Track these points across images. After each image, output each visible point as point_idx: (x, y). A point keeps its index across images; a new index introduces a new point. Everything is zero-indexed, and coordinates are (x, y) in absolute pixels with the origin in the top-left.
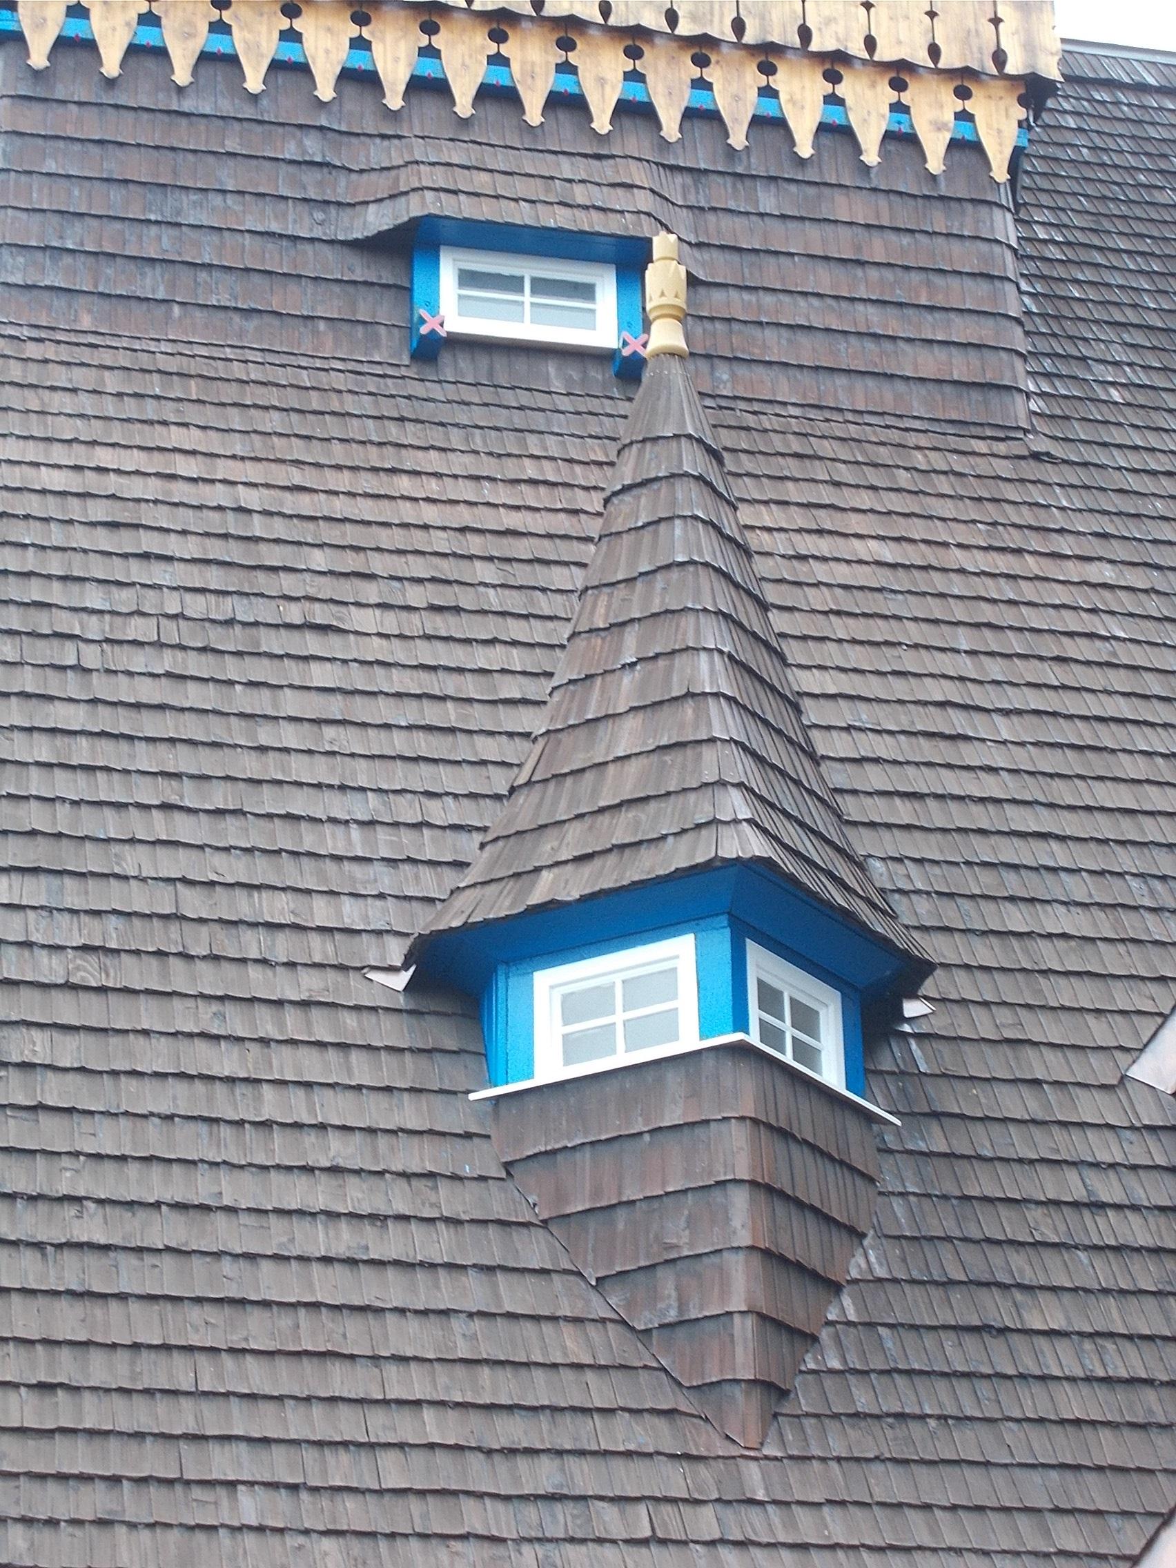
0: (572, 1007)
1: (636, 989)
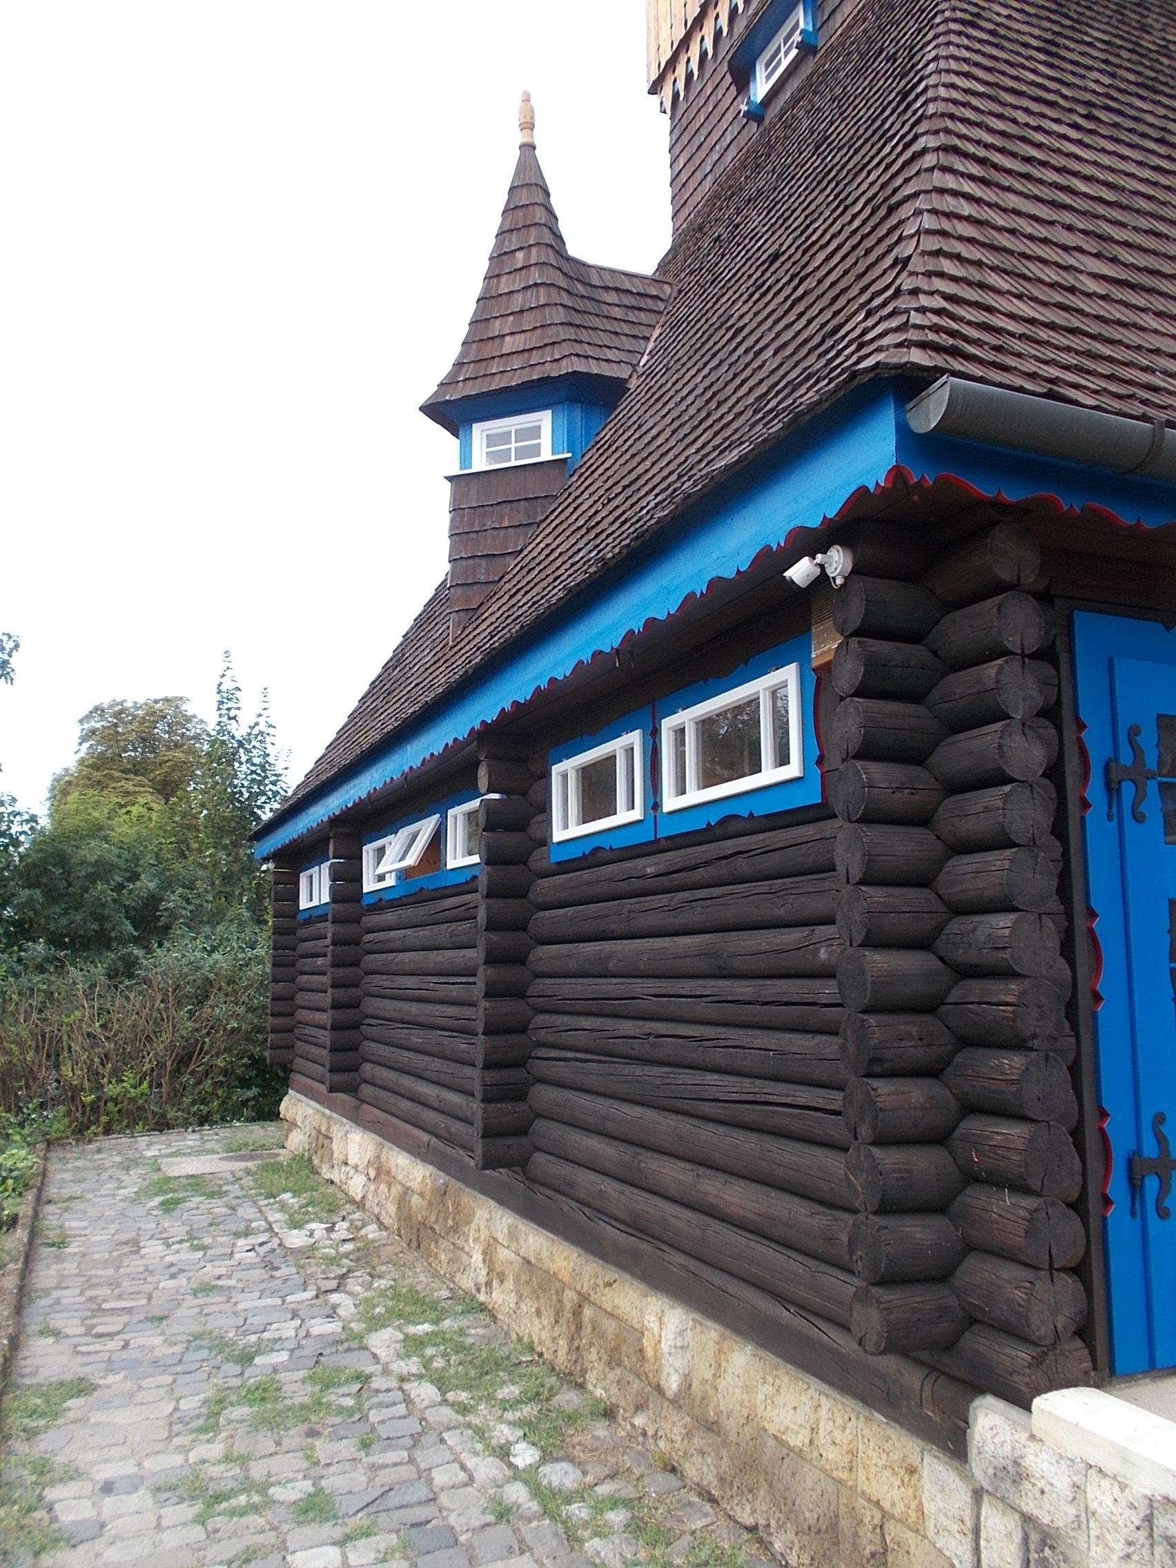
0: (491, 440)
1: (523, 434)
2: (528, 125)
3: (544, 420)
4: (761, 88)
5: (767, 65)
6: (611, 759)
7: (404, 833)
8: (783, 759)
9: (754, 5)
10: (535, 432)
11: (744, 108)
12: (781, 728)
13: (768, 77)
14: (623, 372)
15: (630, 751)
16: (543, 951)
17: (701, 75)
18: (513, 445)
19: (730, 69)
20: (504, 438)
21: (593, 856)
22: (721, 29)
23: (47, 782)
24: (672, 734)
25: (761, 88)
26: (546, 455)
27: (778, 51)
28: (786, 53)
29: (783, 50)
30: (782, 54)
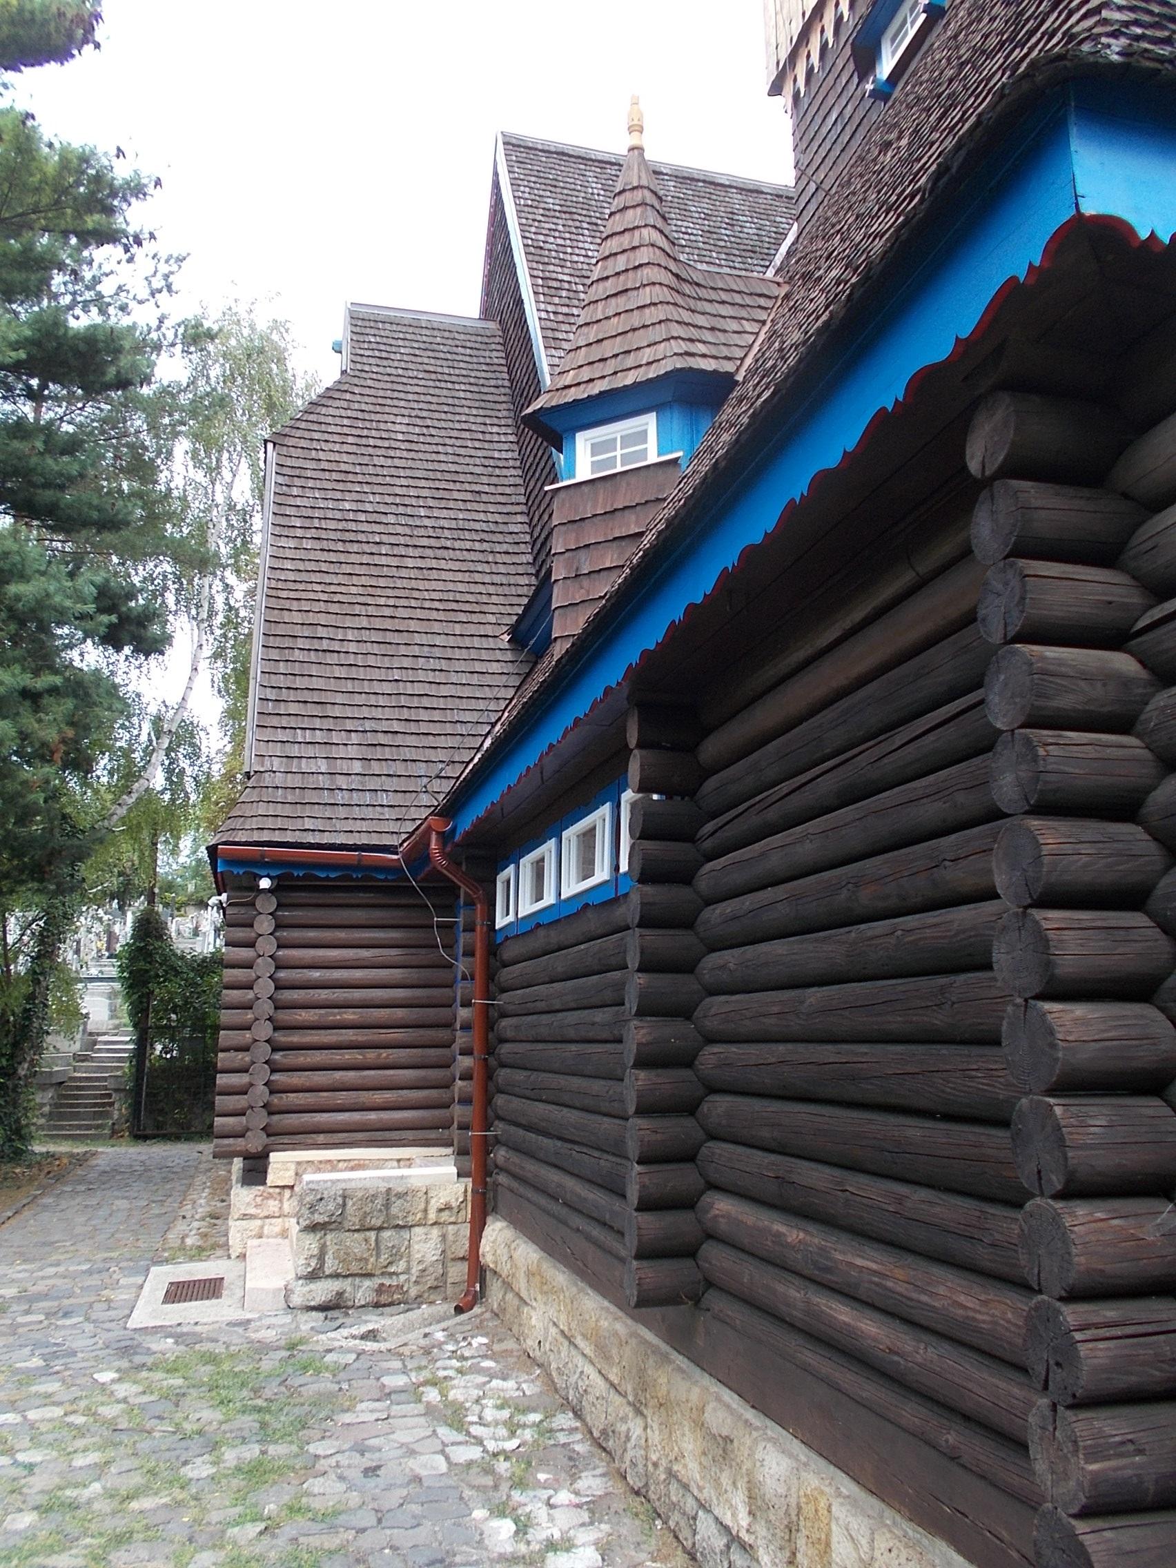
0: (596, 449)
1: (627, 440)
3: (649, 422)
4: (886, 65)
5: (893, 40)
7: (527, 862)
9: (862, 9)
10: (642, 436)
11: (869, 87)
12: (142, 1011)
13: (894, 53)
14: (729, 367)
16: (718, 1003)
17: (822, 67)
18: (619, 453)
19: (853, 54)
20: (609, 445)
21: (536, 924)
22: (827, 42)
23: (70, 65)
24: (629, 807)
25: (886, 65)
26: (653, 458)
27: (904, 22)
28: (913, 23)
29: (909, 20)
30: (908, 25)
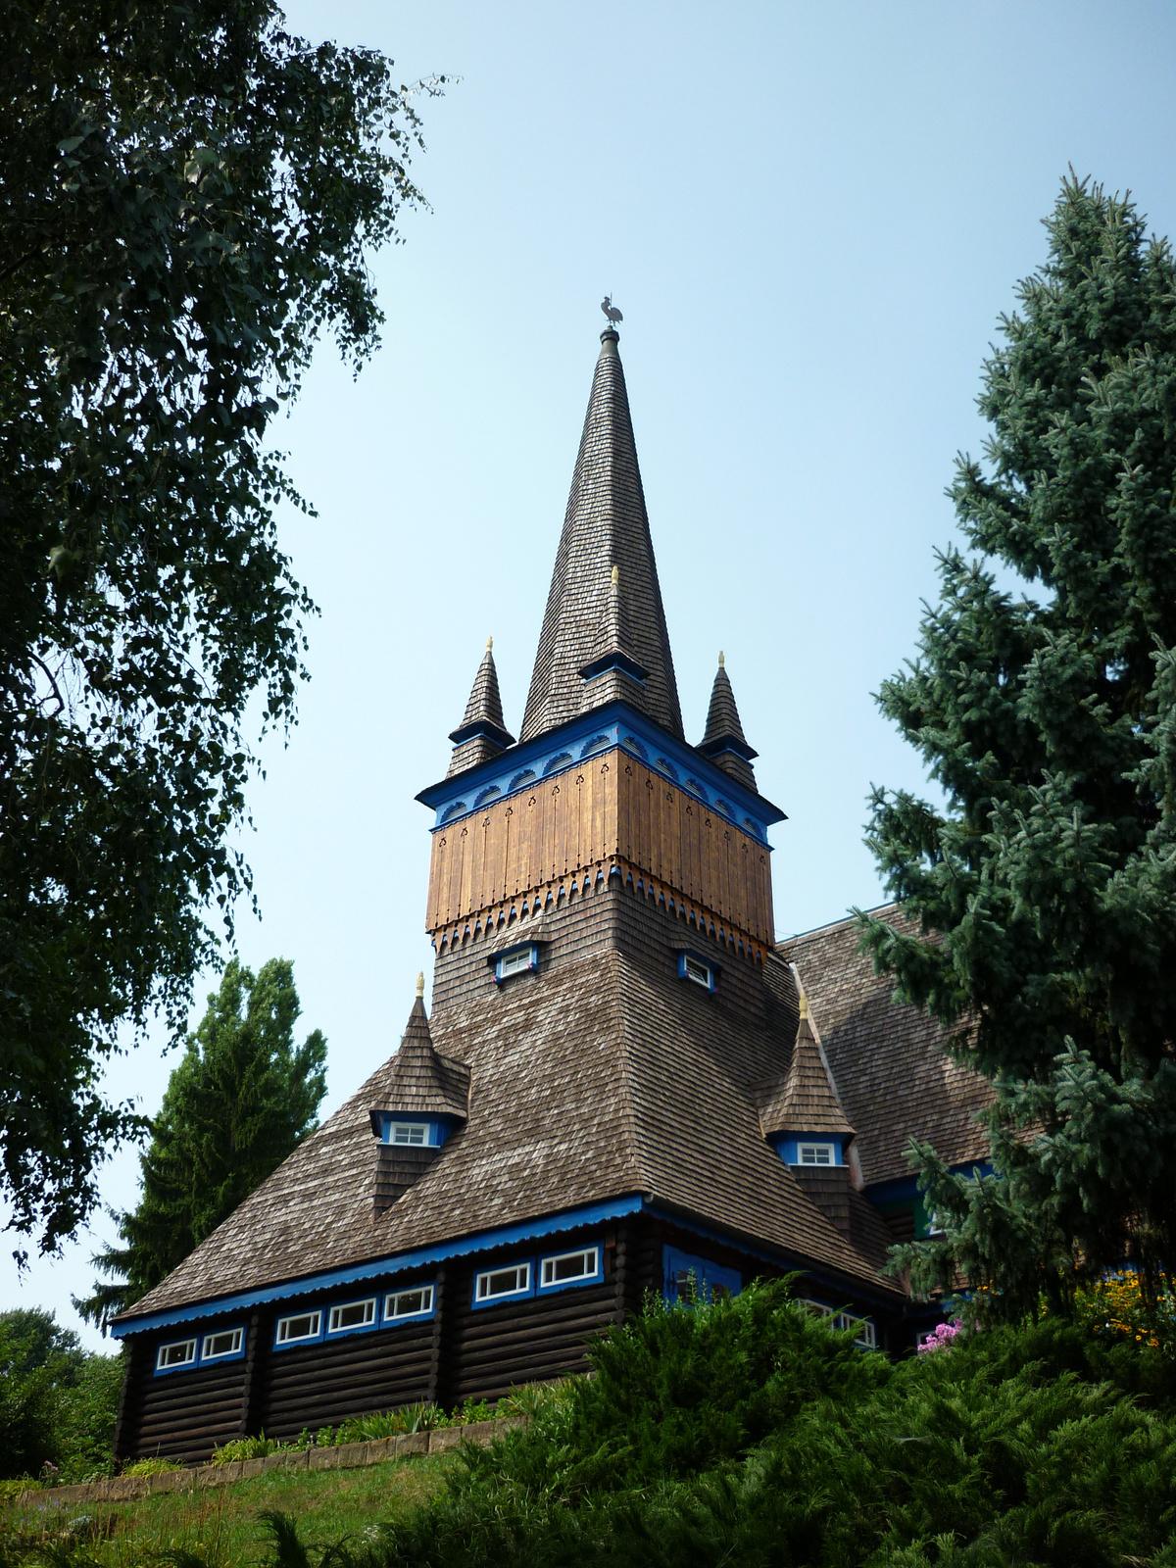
1: (414, 1131)
2: (722, 661)
6: (515, 1273)
8: (369, 1319)
10: (421, 1132)
15: (316, 1318)
